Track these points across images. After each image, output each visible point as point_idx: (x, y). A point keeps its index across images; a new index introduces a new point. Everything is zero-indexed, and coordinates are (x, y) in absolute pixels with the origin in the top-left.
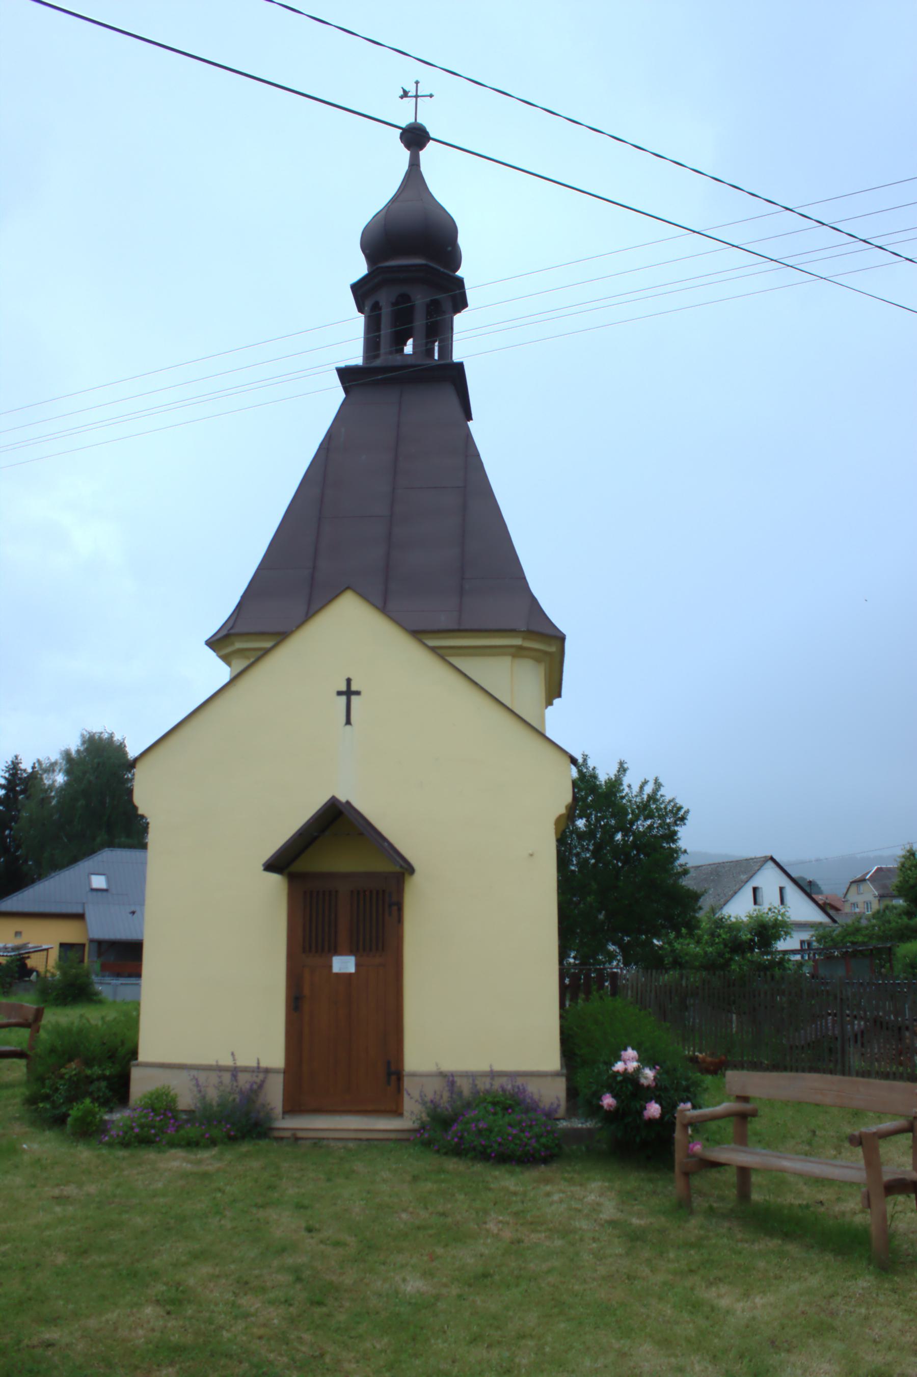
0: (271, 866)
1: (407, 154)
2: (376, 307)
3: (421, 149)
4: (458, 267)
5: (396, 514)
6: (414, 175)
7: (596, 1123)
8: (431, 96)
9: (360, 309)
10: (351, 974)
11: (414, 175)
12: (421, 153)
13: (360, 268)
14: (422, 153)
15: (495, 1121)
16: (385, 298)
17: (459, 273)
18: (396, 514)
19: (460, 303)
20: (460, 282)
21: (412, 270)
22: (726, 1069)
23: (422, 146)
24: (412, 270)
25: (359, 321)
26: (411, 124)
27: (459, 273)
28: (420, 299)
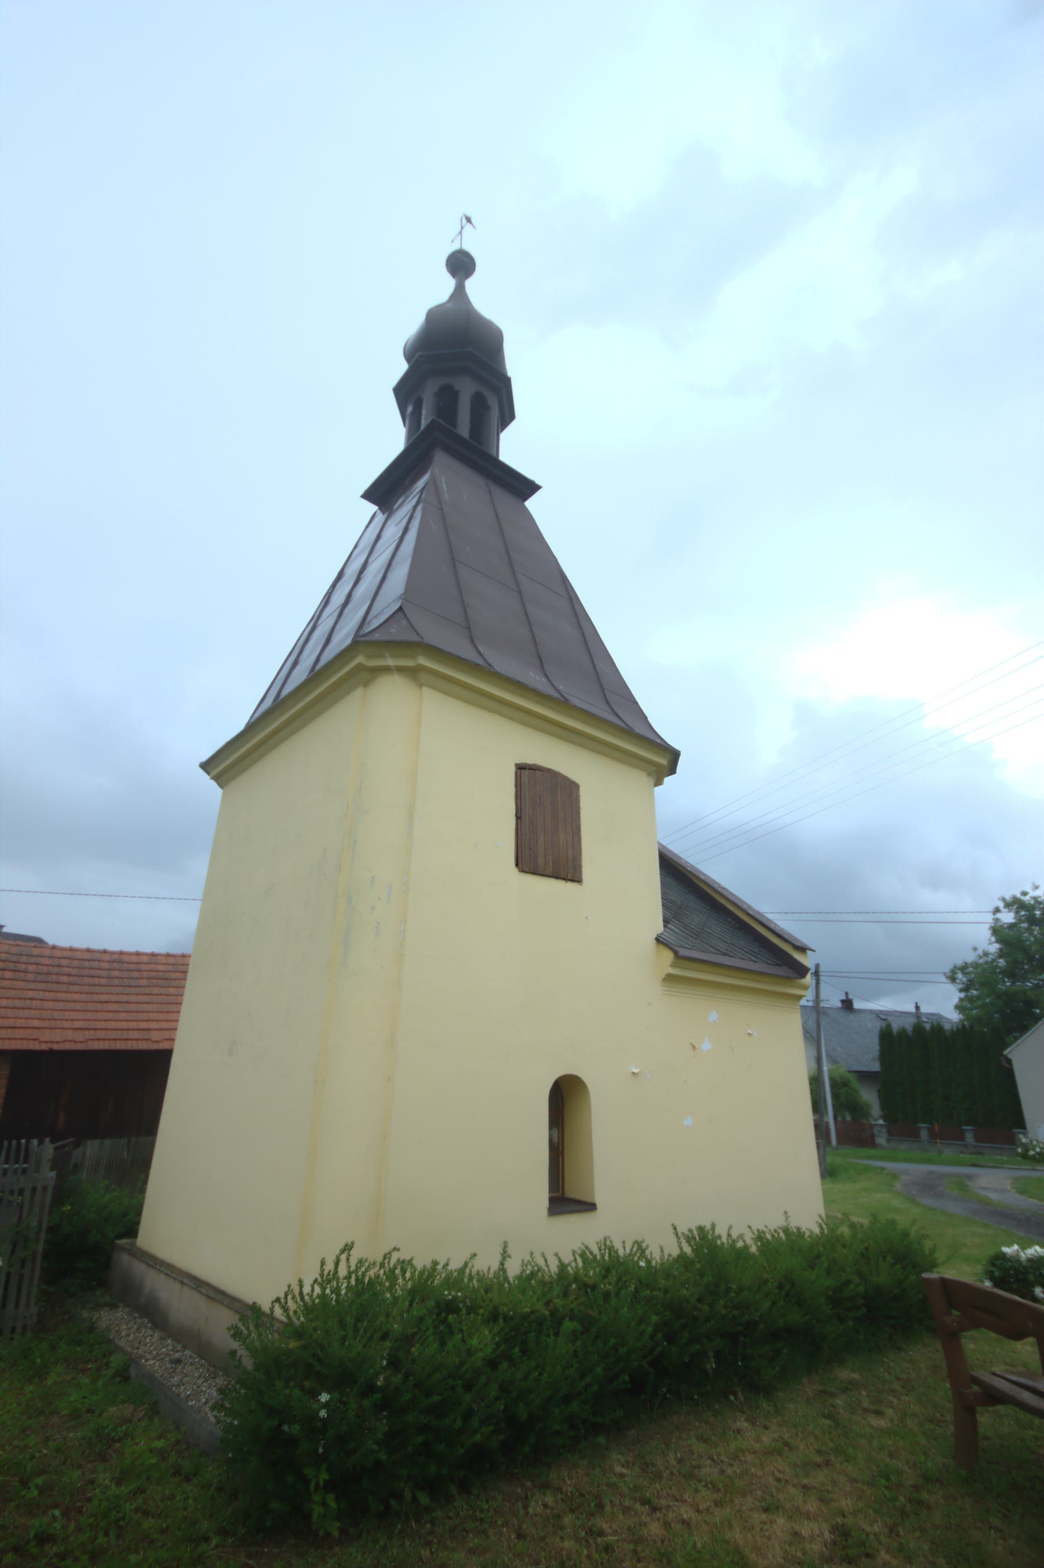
6: (459, 292)
11: (459, 292)
19: (507, 415)
24: (456, 382)
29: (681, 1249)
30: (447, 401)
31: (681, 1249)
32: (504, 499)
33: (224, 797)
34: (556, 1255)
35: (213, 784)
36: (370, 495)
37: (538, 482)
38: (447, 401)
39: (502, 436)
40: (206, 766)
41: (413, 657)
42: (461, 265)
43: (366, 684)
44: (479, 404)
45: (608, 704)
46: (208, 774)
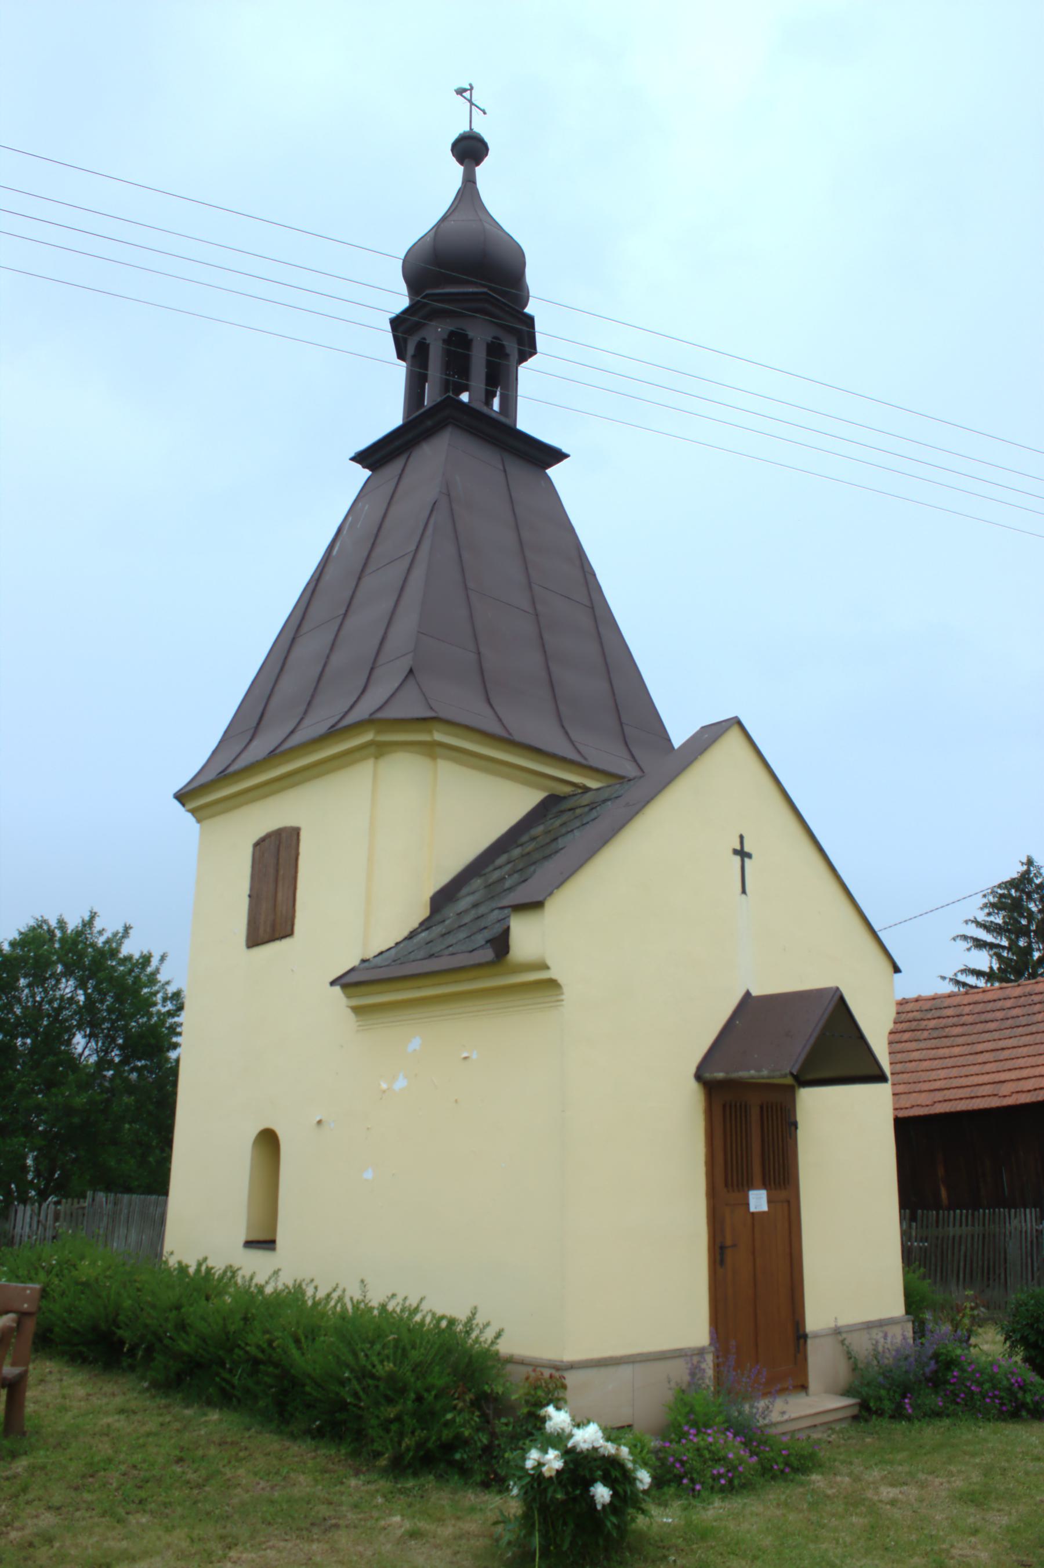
0: (362, 458)
1: (460, 169)
2: (422, 349)
3: (478, 164)
4: (525, 305)
5: (459, 599)
6: (469, 188)
7: (244, 1277)
8: (485, 113)
9: (401, 355)
10: (764, 1213)
11: (469, 188)
12: (477, 169)
13: (401, 301)
14: (479, 170)
15: (829, 1436)
16: (435, 334)
17: (527, 310)
18: (459, 599)
19: (527, 348)
20: (530, 321)
21: (466, 307)
22: (749, 1190)
23: (478, 161)
24: (466, 307)
25: (399, 371)
26: (465, 133)
27: (527, 310)
28: (480, 334)
29: (267, 1283)
30: (458, 349)
31: (267, 1283)
32: (519, 471)
33: (201, 828)
34: (966, 922)
35: (189, 815)
36: (362, 458)
37: (565, 450)
38: (458, 349)
39: (519, 368)
40: (182, 797)
41: (430, 732)
42: (470, 150)
43: (378, 756)
44: (495, 350)
45: (635, 761)
46: (183, 805)
